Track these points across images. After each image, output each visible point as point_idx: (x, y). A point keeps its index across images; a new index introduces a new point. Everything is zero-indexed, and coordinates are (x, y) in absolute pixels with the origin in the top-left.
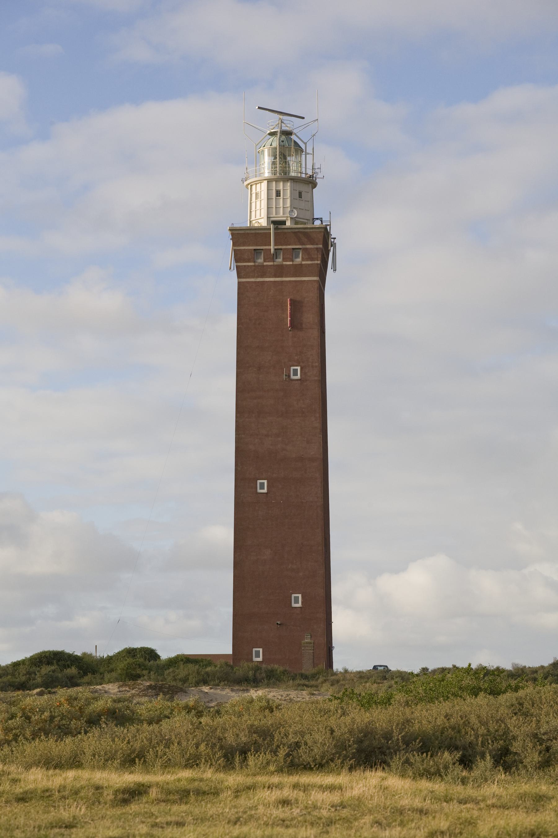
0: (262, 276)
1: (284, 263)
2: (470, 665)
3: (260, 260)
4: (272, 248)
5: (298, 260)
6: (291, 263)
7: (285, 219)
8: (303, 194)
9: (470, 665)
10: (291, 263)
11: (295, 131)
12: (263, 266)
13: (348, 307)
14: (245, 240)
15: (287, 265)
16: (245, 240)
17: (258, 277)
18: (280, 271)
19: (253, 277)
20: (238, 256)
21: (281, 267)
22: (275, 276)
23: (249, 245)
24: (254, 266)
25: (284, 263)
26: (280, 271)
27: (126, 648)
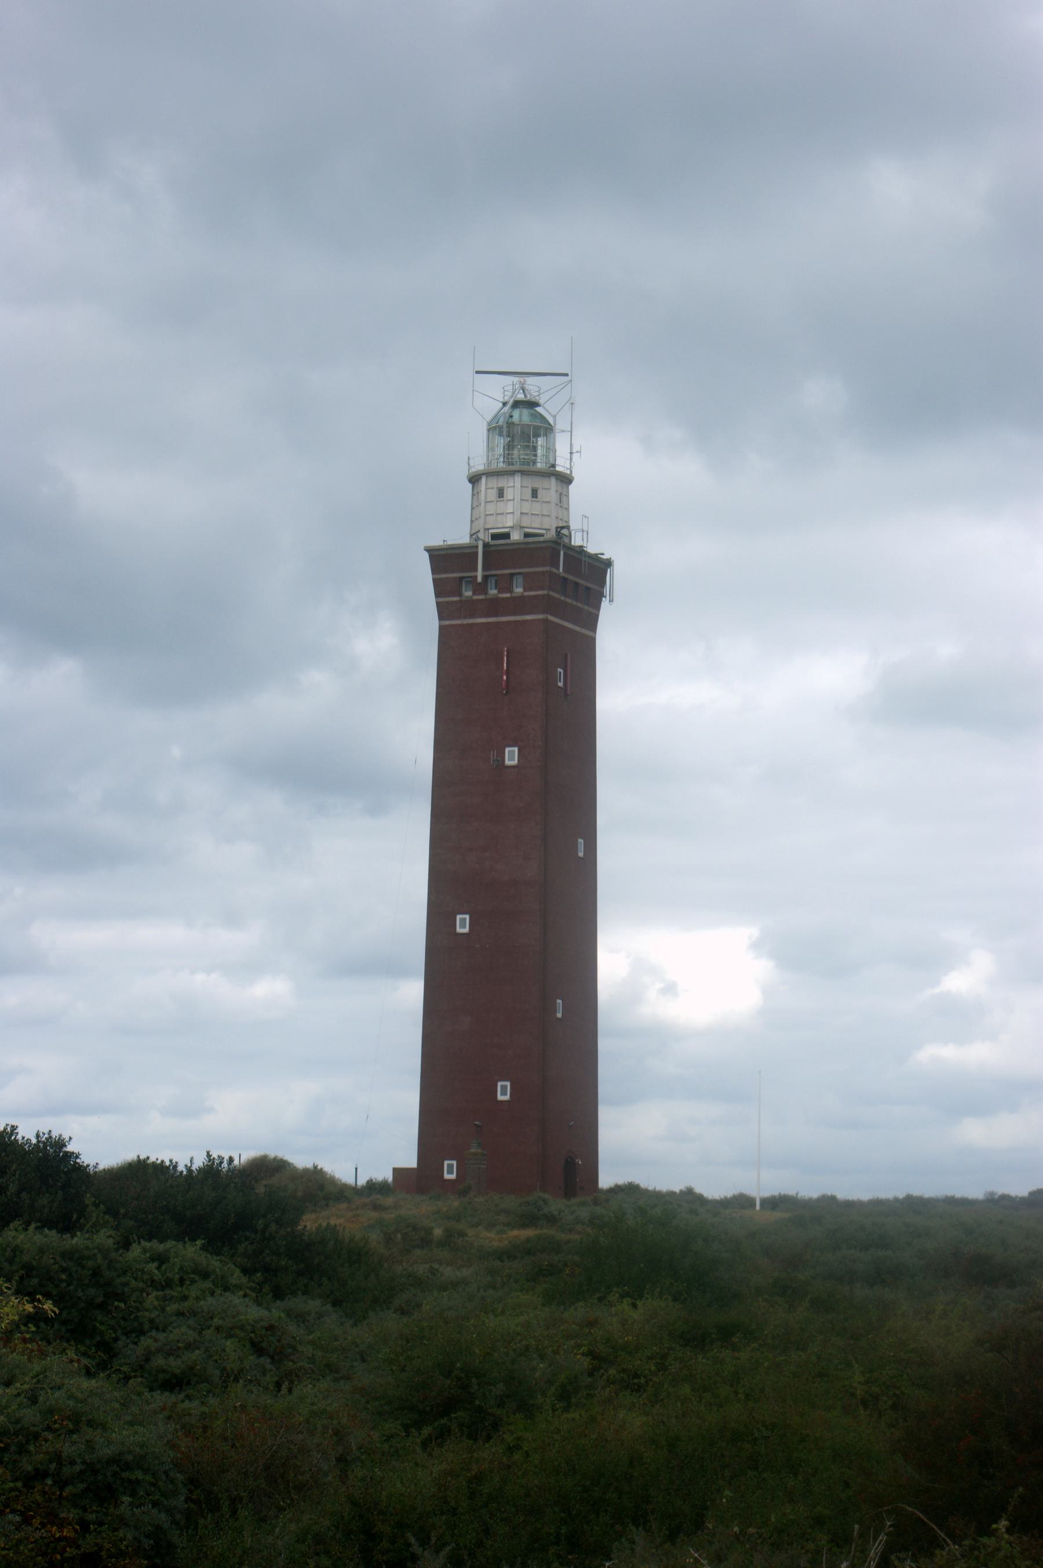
0: (471, 616)
1: (501, 595)
2: (208, 1155)
3: (468, 593)
4: (479, 575)
5: (519, 590)
6: (508, 595)
7: (507, 530)
8: (540, 493)
9: (208, 1155)
10: (508, 595)
11: (541, 402)
12: (473, 601)
13: (648, 690)
14: (447, 562)
15: (503, 599)
16: (447, 562)
17: (465, 618)
18: (494, 607)
19: (459, 618)
20: (440, 588)
21: (495, 601)
22: (487, 615)
23: (453, 572)
24: (460, 601)
25: (501, 595)
26: (494, 607)
27: (833, 1198)
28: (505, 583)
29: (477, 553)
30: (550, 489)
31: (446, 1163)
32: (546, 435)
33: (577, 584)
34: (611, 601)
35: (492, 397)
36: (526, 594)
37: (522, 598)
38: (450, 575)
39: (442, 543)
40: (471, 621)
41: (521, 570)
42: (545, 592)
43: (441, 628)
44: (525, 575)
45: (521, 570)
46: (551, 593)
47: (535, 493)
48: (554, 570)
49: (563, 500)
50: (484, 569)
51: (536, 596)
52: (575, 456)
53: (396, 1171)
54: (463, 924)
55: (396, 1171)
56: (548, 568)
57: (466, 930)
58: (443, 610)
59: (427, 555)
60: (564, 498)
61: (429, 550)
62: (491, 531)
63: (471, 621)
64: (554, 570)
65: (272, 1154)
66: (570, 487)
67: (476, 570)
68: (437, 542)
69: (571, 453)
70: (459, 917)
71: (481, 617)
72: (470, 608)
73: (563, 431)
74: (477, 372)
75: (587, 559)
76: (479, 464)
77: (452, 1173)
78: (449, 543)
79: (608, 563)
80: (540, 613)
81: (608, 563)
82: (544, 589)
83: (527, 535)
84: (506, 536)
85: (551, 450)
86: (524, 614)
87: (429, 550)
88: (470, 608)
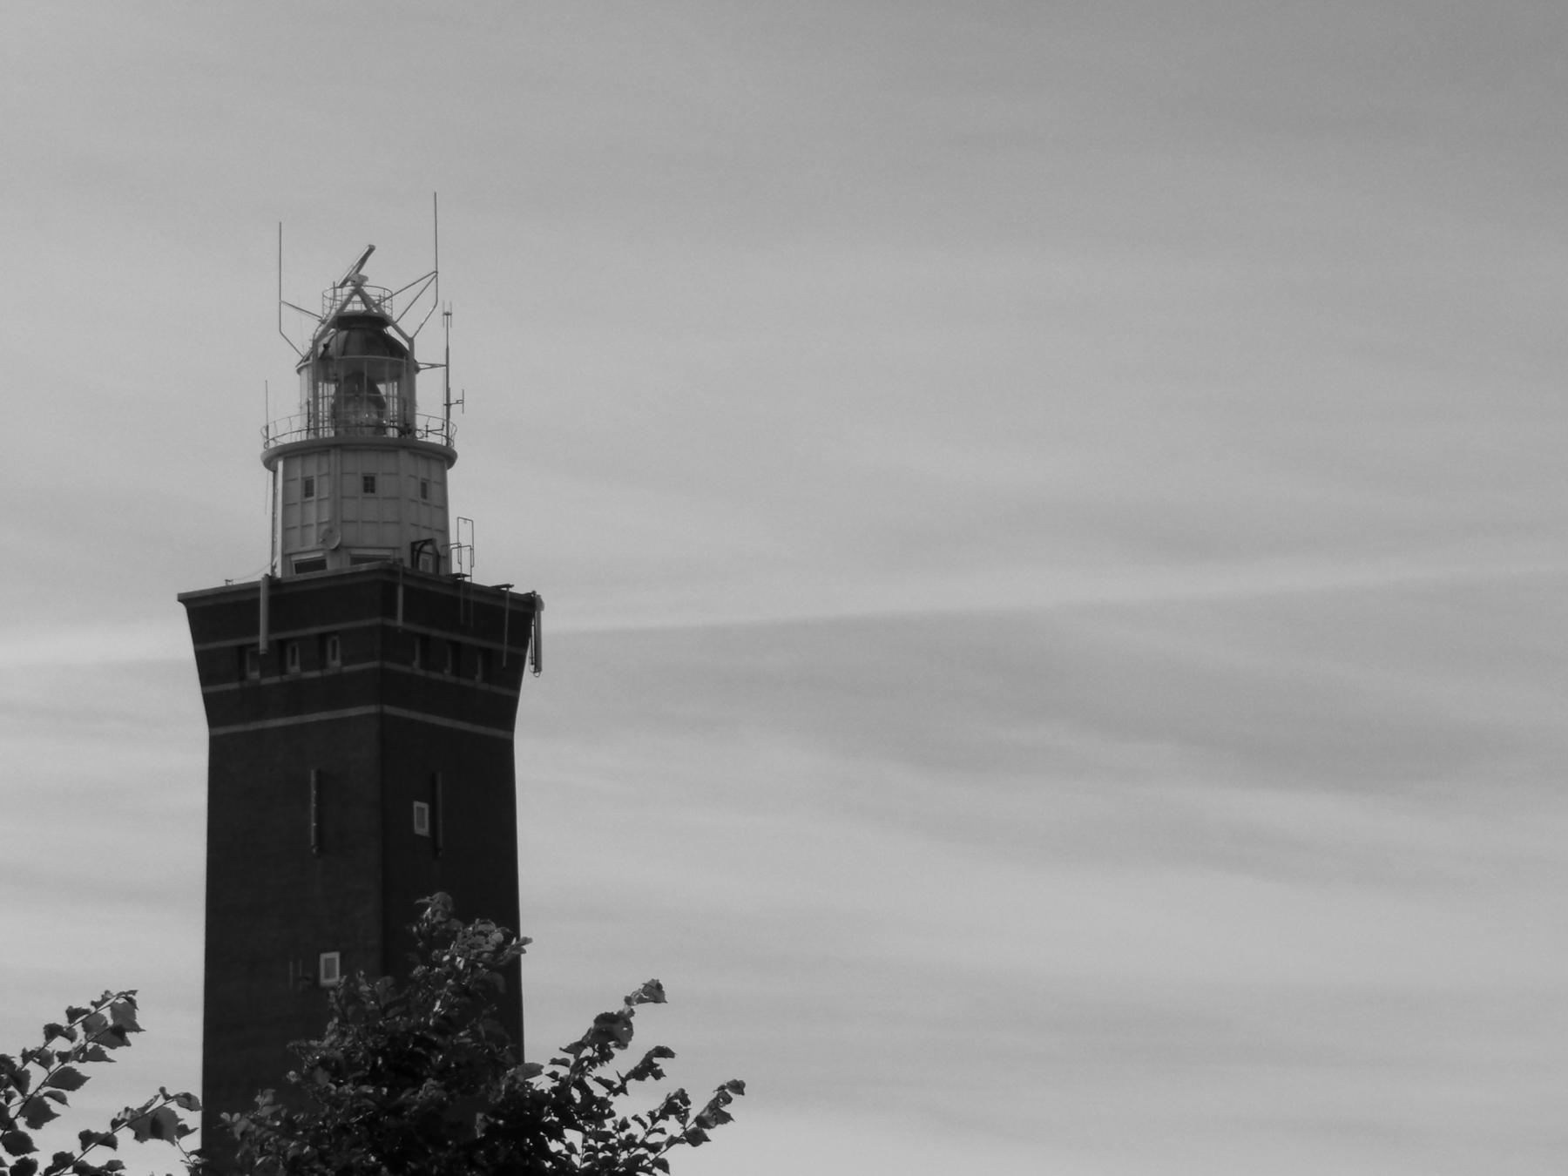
4: (262, 640)
8: (381, 483)
20: (210, 668)
22: (287, 713)
26: (297, 697)
29: (257, 601)
30: (398, 474)
32: (397, 377)
33: (457, 646)
34: (538, 668)
35: (314, 299)
36: (346, 669)
39: (223, 584)
42: (376, 664)
46: (389, 665)
47: (369, 484)
48: (389, 622)
49: (433, 496)
50: (272, 628)
52: (453, 408)
56: (377, 620)
59: (182, 609)
60: (434, 490)
61: (187, 600)
62: (296, 558)
64: (389, 622)
66: (450, 473)
67: (256, 632)
68: (209, 580)
69: (448, 405)
71: (276, 716)
73: (433, 366)
74: (371, 249)
75: (473, 598)
76: (292, 430)
78: (235, 582)
79: (529, 606)
81: (529, 606)
83: (357, 560)
84: (319, 564)
85: (408, 402)
87: (187, 600)
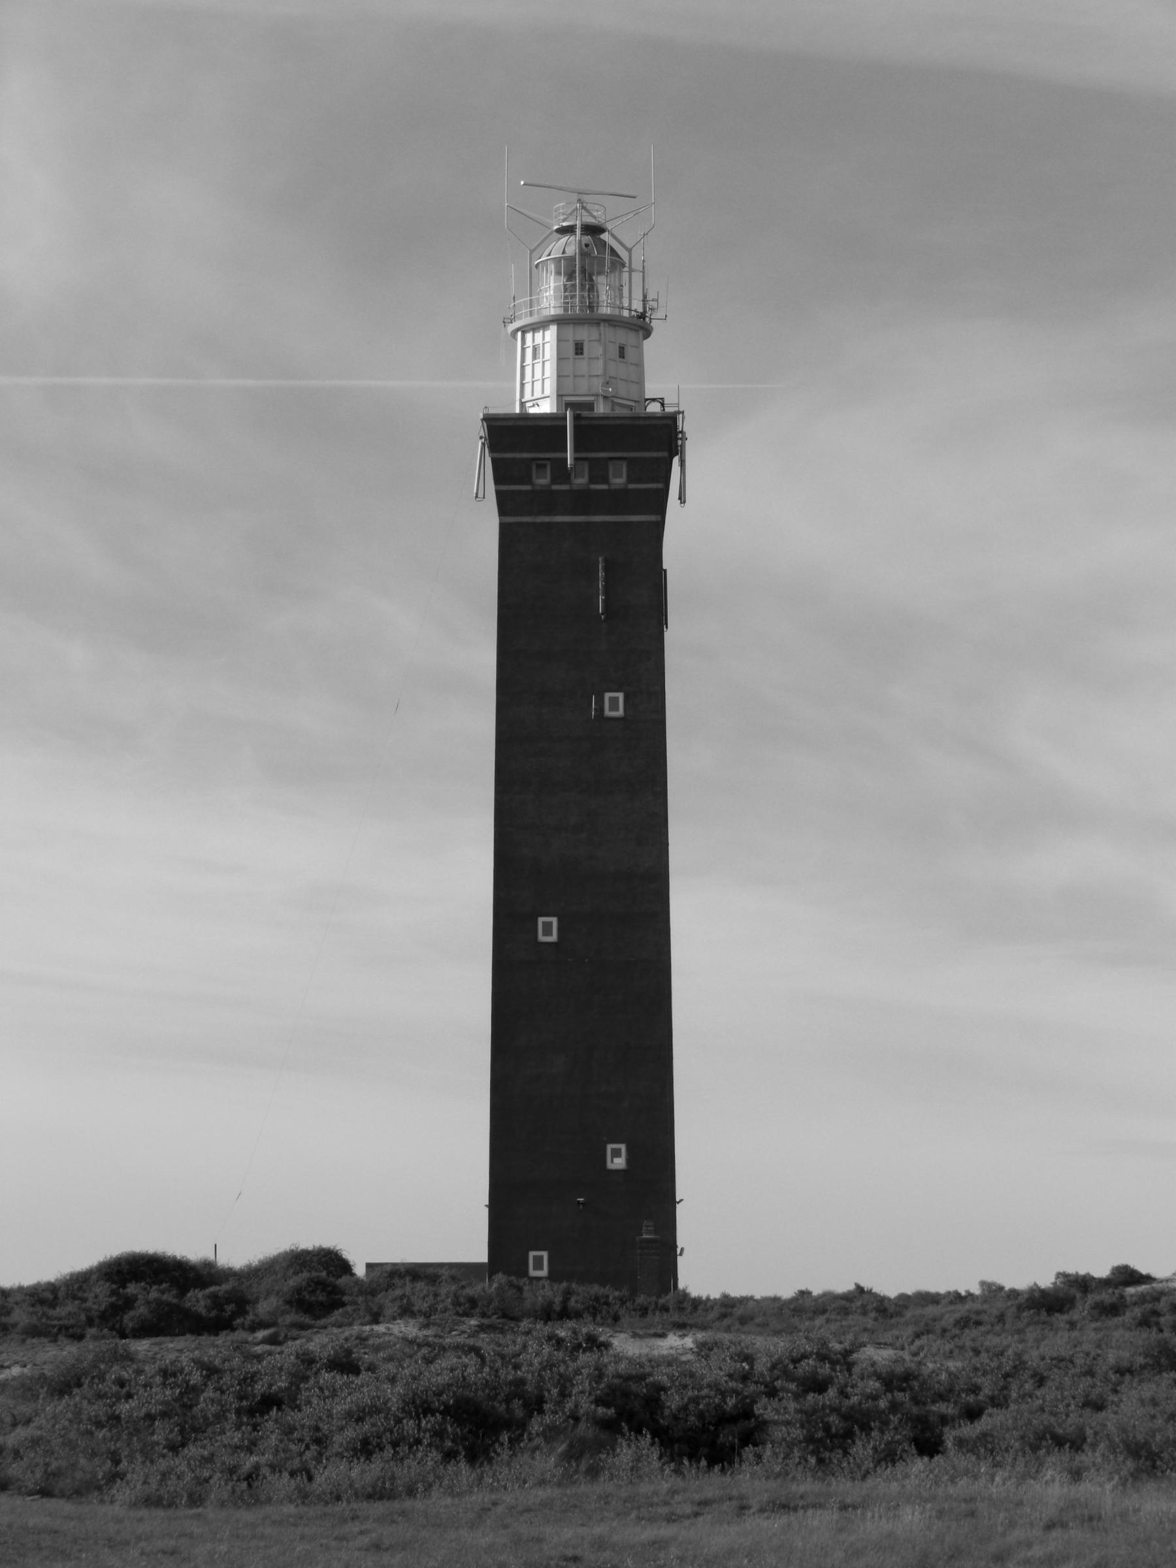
0: (549, 512)
7: (592, 398)
10: (604, 487)
11: (609, 226)
15: (558, 492)
17: (539, 514)
18: (583, 501)
19: (530, 514)
23: (522, 451)
28: (599, 472)
31: (532, 1254)
34: (682, 498)
36: (631, 486)
37: (625, 492)
38: (518, 455)
40: (547, 519)
41: (625, 455)
43: (503, 526)
44: (631, 462)
45: (625, 455)
50: (577, 449)
51: (646, 490)
53: (983, 1284)
54: (548, 929)
55: (983, 1284)
57: (554, 938)
58: (505, 504)
63: (547, 519)
65: (346, 1255)
70: (541, 920)
71: (562, 514)
72: (547, 501)
77: (541, 1268)
80: (652, 514)
82: (658, 482)
86: (628, 514)
88: (547, 501)
